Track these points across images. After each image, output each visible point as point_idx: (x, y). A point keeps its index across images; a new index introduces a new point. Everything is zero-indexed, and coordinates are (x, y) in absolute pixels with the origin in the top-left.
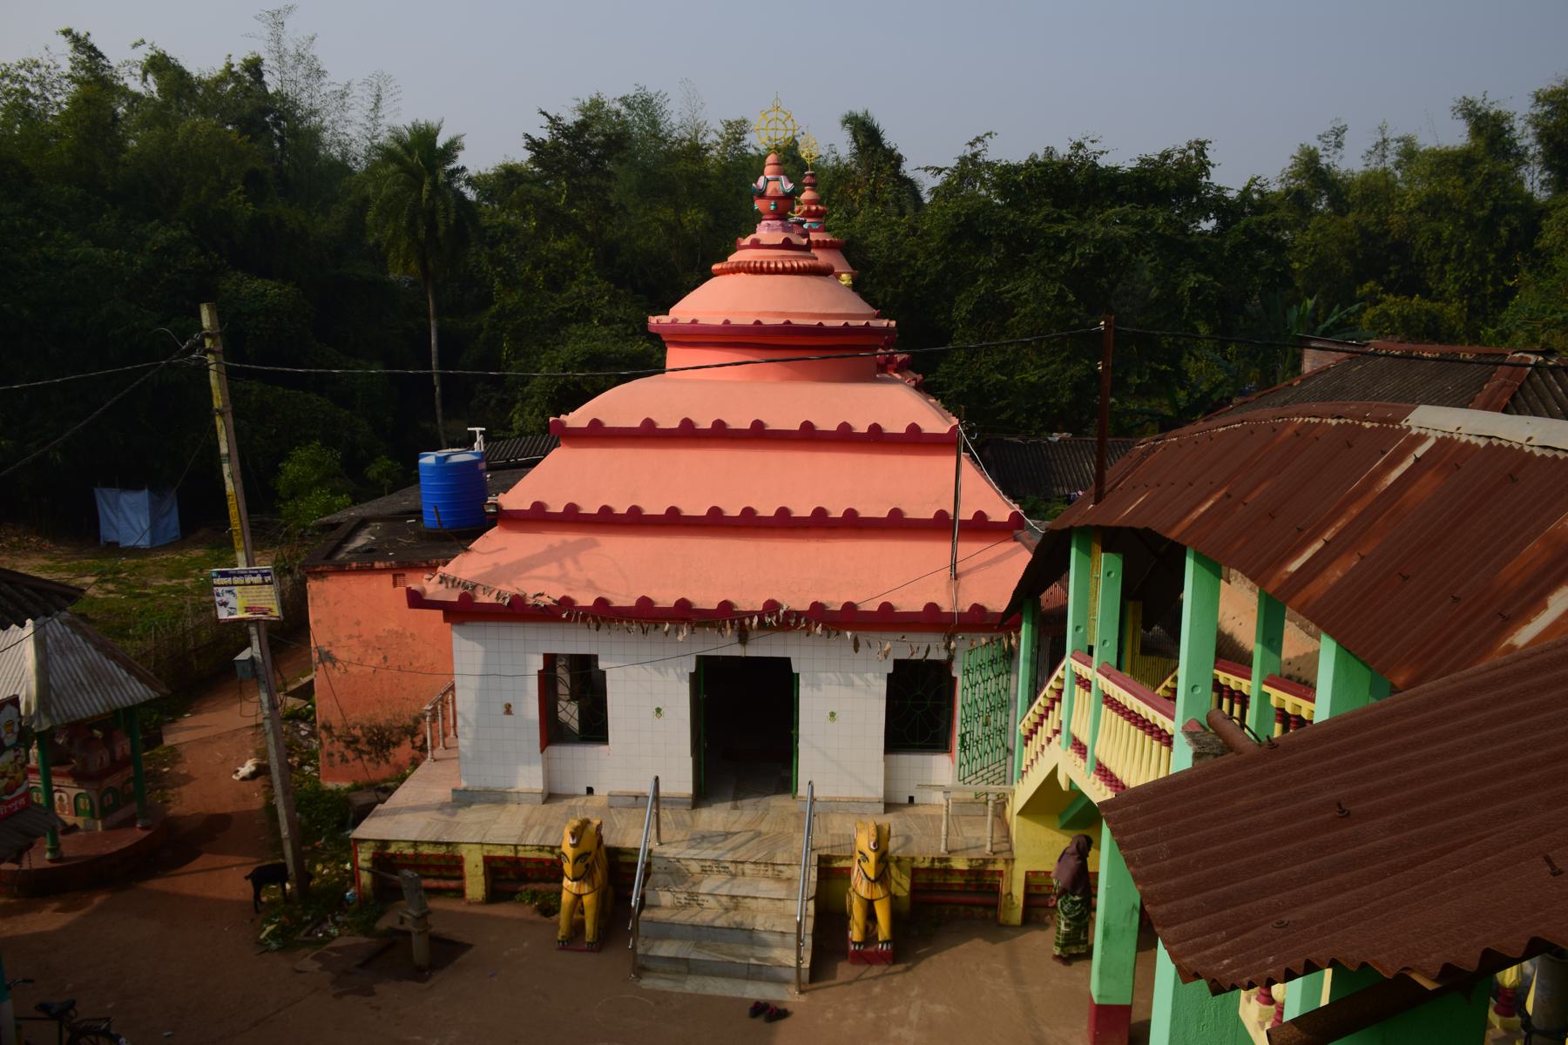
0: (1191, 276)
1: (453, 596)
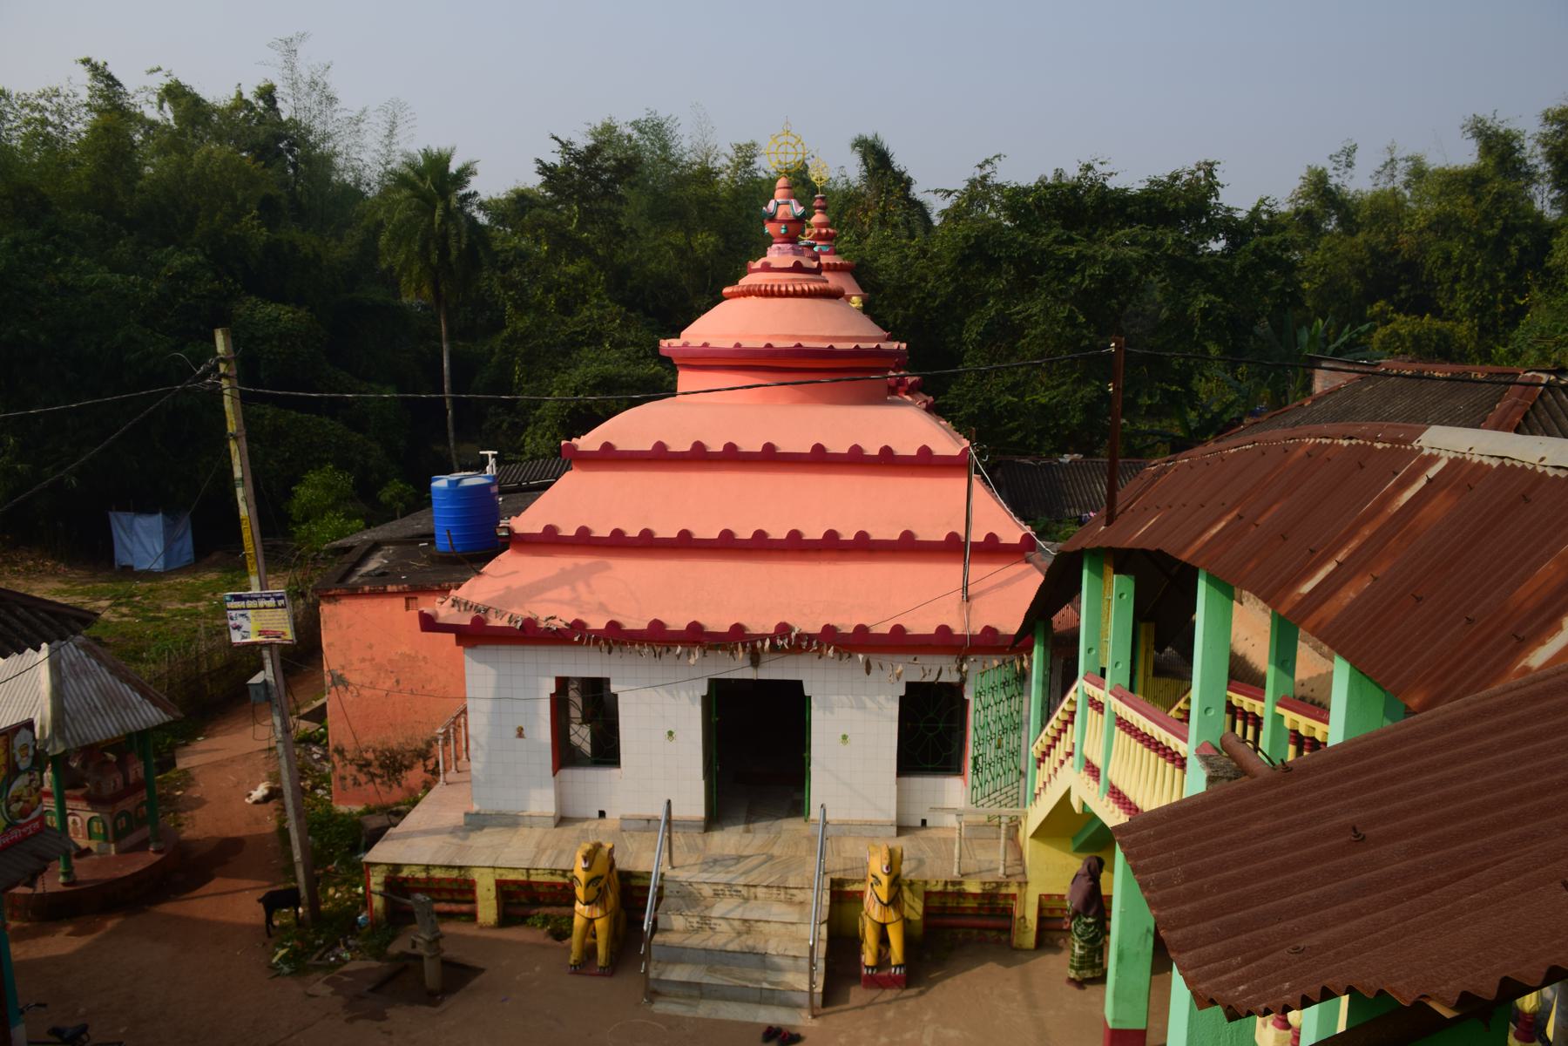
0: (1201, 297)
1: (466, 619)
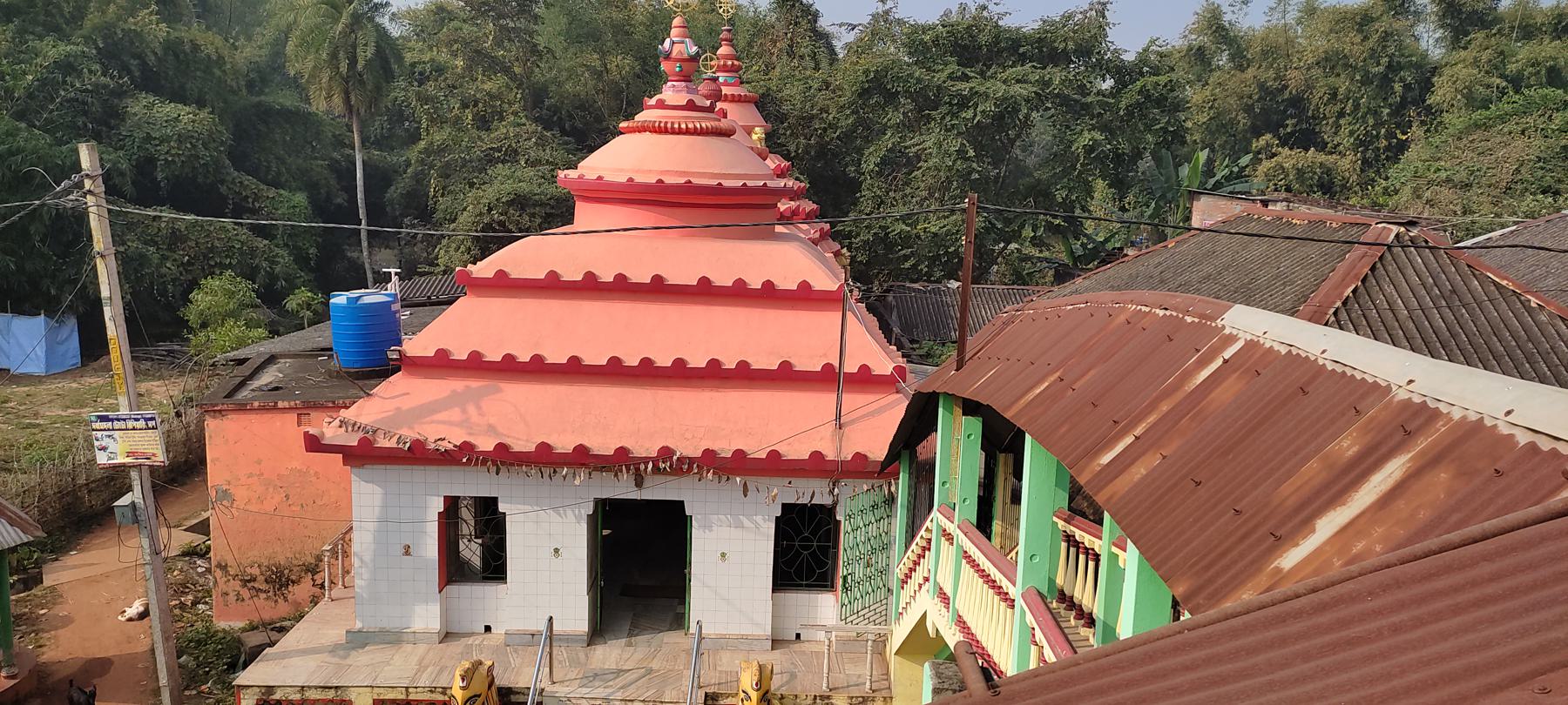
0: (1086, 133)
